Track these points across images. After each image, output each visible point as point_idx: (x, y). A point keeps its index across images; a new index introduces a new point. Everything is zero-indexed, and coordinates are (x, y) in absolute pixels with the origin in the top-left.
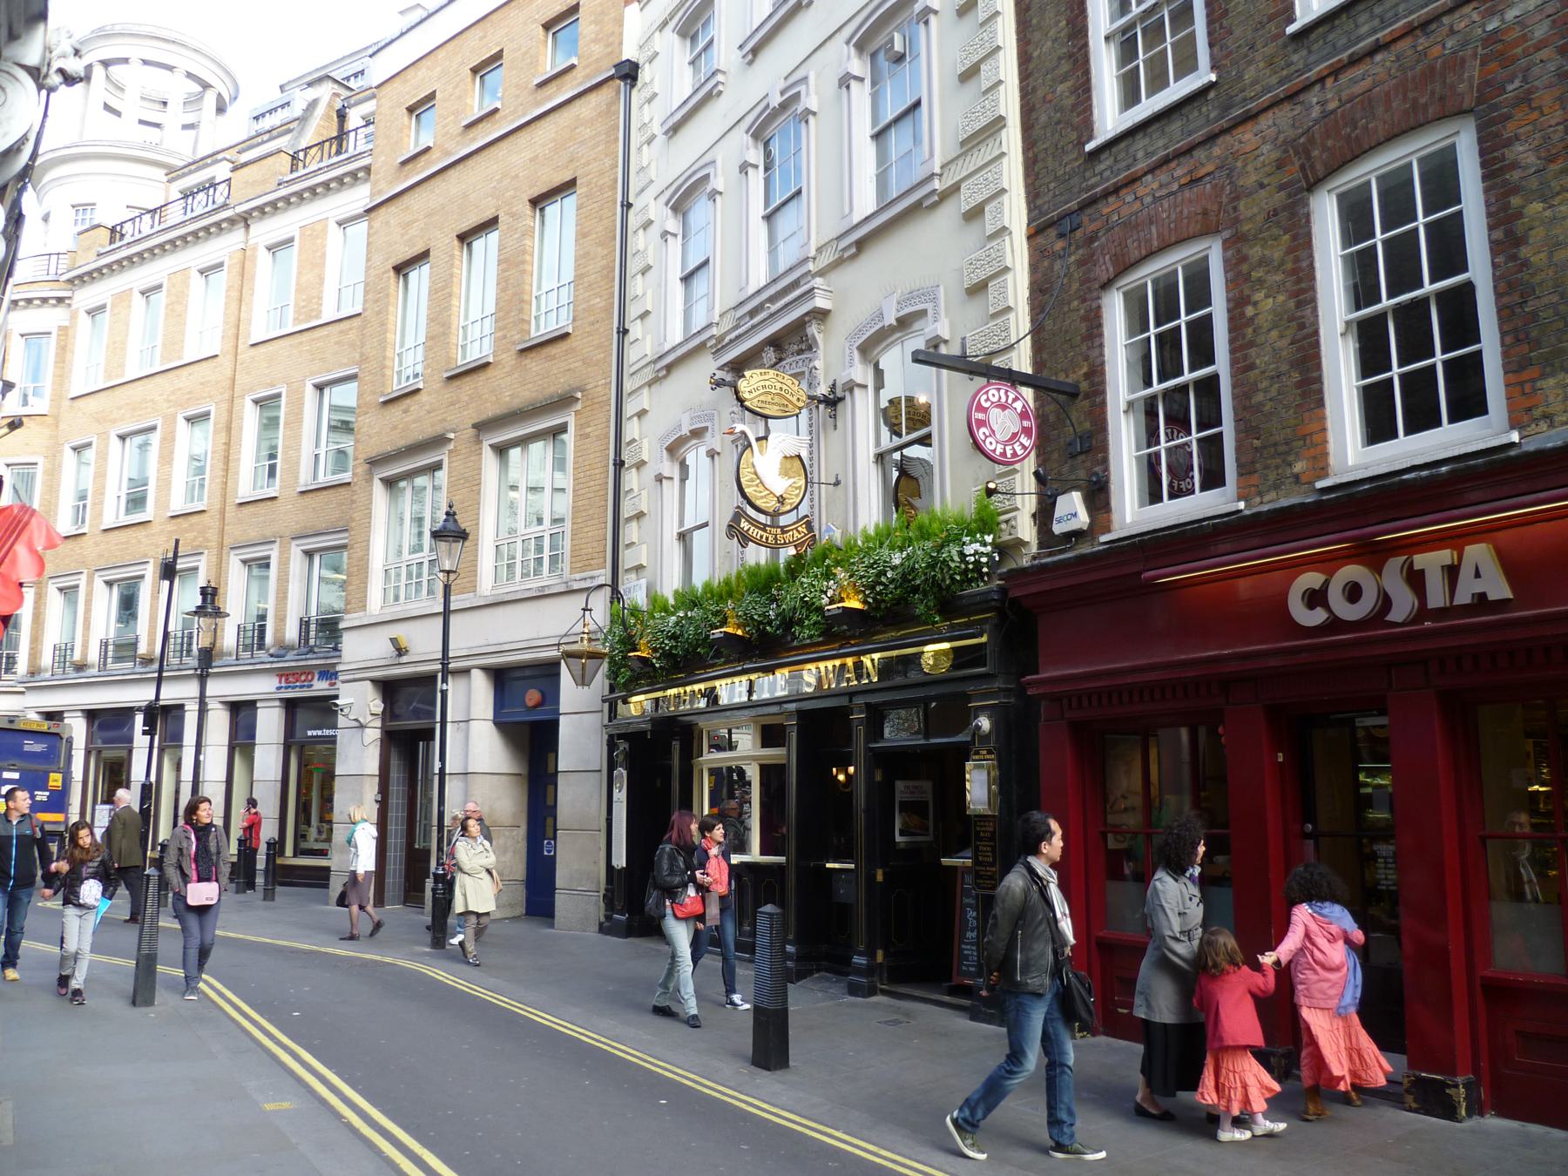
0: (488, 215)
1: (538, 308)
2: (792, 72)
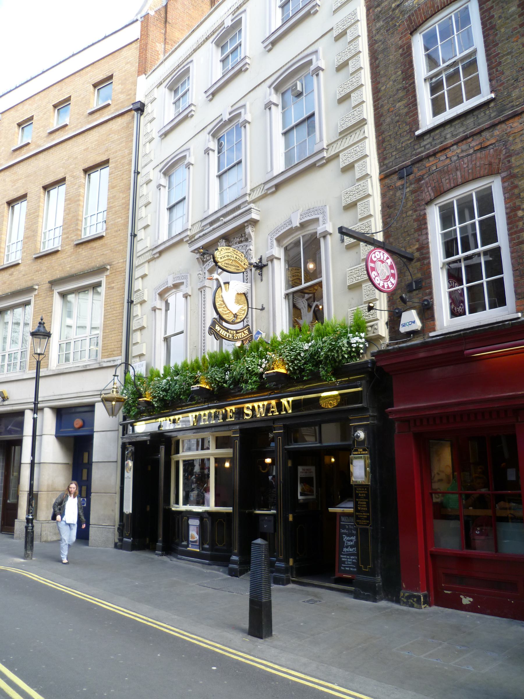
0: (60, 176)
1: (86, 224)
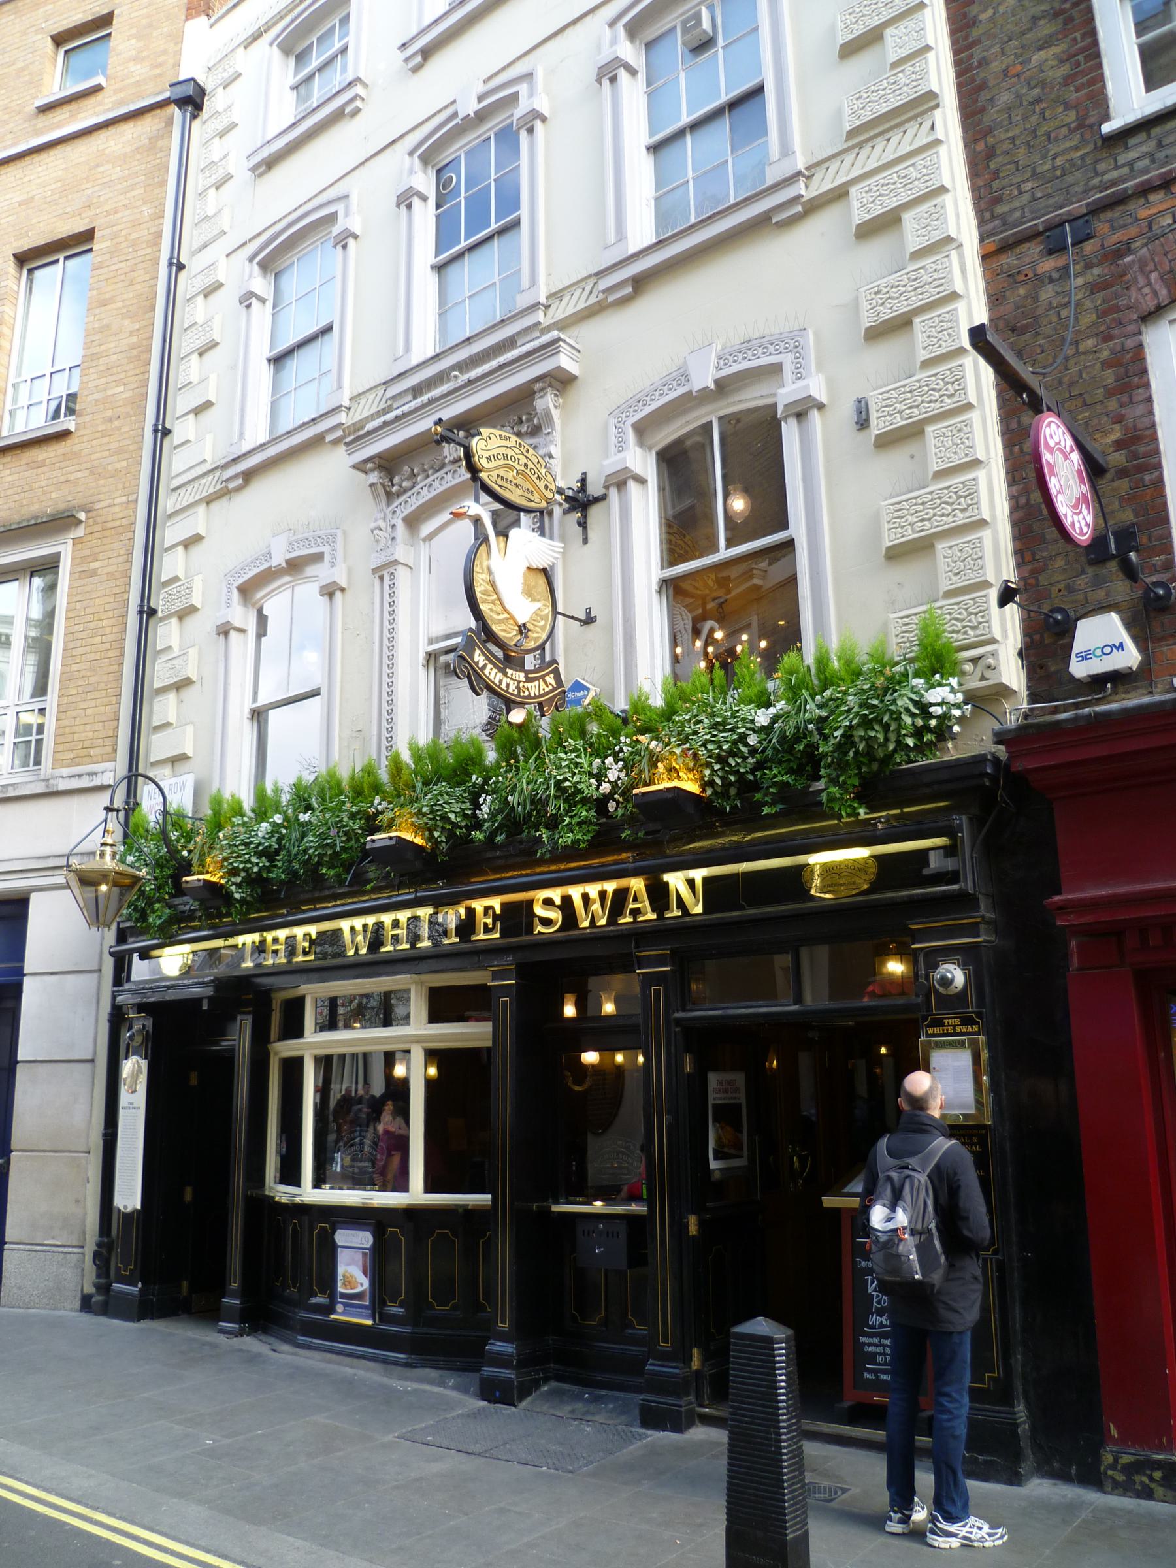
1: (15, 401)
2: (509, 65)
